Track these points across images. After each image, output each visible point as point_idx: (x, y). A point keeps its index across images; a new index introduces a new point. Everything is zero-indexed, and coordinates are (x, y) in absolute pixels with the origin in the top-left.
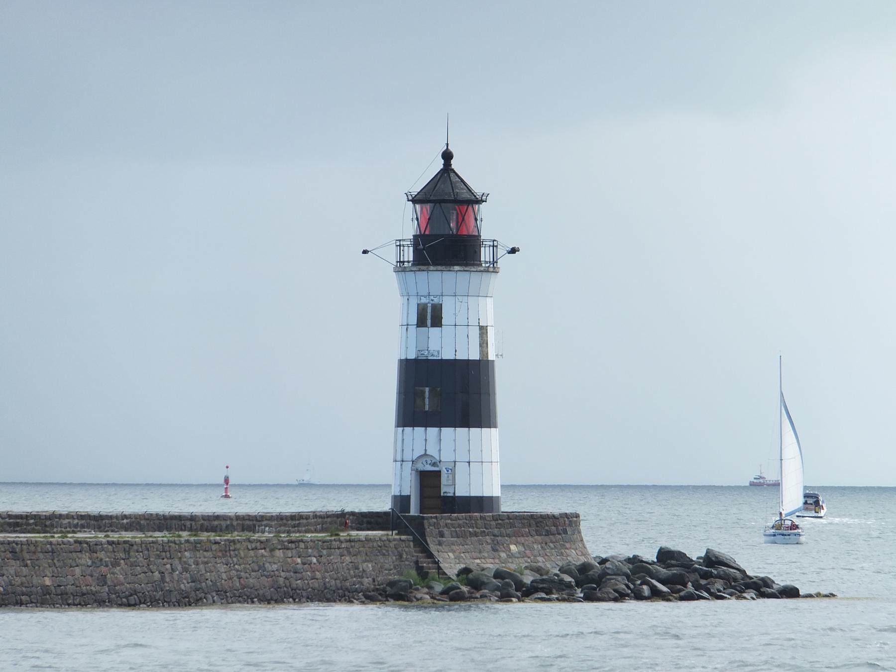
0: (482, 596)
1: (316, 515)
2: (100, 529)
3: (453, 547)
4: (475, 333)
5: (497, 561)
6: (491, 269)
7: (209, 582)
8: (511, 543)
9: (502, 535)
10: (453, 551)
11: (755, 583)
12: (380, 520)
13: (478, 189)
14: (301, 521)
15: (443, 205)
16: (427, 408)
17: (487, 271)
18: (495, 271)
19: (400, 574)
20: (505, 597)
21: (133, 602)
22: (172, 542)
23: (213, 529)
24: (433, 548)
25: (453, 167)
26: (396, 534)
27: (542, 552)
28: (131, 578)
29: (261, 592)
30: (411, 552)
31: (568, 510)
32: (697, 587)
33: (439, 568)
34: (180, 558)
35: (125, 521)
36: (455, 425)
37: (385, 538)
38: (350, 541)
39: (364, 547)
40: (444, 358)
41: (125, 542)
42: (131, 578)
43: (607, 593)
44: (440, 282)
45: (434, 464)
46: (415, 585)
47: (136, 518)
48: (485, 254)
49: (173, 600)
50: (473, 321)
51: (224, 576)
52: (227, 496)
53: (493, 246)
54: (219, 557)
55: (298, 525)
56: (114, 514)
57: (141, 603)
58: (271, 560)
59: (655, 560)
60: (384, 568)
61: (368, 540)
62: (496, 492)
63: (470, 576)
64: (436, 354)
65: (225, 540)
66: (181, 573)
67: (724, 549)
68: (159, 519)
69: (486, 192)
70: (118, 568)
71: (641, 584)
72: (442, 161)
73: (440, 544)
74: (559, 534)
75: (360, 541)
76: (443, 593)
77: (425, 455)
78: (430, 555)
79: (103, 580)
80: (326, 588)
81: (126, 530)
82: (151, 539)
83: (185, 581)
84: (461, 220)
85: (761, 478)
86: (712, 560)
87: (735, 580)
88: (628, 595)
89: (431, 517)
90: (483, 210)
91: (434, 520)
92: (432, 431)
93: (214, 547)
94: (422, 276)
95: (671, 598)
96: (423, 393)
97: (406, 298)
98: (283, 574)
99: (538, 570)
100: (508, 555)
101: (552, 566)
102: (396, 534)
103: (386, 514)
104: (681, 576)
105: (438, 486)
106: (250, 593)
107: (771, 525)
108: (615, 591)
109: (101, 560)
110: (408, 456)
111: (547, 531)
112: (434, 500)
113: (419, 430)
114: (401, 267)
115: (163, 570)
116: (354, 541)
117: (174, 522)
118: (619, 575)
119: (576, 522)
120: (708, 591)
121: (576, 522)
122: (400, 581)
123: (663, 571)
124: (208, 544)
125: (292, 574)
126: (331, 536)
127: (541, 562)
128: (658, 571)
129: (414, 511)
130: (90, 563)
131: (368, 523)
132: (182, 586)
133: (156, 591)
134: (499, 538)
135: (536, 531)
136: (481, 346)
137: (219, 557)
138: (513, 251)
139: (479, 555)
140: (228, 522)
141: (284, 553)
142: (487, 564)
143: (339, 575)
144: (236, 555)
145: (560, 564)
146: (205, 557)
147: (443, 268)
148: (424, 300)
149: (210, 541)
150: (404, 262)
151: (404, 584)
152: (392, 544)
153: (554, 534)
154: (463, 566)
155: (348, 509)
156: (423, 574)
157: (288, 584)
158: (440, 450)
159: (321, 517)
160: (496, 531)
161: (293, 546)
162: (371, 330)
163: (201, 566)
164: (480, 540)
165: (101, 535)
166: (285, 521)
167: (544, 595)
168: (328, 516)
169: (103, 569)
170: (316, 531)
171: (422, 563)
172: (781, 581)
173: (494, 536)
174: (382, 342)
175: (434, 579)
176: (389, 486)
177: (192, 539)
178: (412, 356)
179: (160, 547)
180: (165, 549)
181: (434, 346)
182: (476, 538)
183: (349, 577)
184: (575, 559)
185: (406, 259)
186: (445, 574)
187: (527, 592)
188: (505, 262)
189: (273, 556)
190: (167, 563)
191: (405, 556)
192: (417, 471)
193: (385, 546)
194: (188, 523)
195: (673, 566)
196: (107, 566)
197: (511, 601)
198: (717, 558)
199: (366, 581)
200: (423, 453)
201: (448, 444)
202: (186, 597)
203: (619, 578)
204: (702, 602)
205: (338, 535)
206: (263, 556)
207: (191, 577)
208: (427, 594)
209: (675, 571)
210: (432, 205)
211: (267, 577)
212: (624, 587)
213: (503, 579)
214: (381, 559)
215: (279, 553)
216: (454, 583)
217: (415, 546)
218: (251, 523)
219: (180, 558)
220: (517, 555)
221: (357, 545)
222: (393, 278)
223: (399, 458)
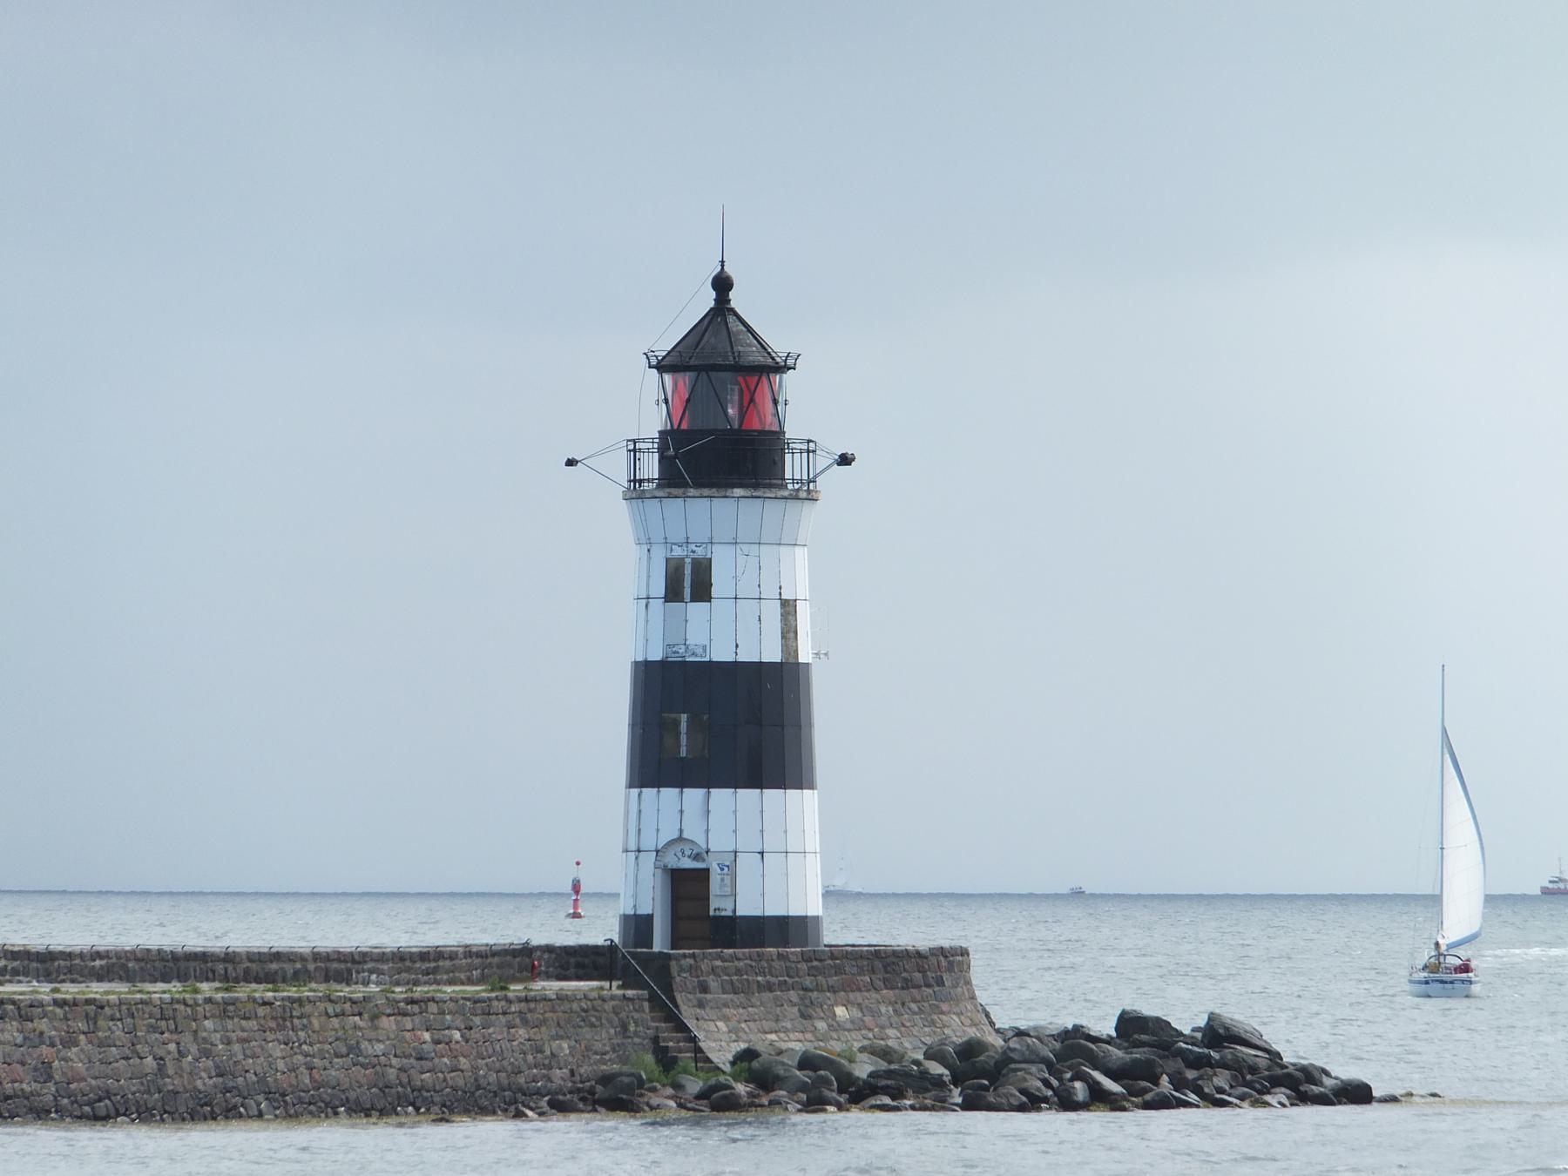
0: (771, 1103)
1: (469, 952)
2: (48, 976)
3: (726, 1011)
4: (773, 612)
5: (809, 1036)
6: (803, 495)
7: (251, 1077)
9: (818, 988)
10: (726, 1019)
11: (1289, 1075)
12: (601, 960)
13: (779, 345)
14: (441, 963)
15: (713, 374)
16: (683, 752)
17: (795, 497)
18: (811, 497)
19: (624, 1060)
20: (814, 1104)
21: (103, 1113)
22: (178, 1002)
23: (269, 979)
24: (688, 1014)
25: (733, 304)
26: (619, 987)
27: (895, 1020)
28: (98, 1068)
29: (352, 1095)
30: (645, 1021)
32: (1179, 1083)
33: (698, 1050)
34: (196, 1032)
35: (98, 963)
36: (735, 784)
37: (594, 994)
38: (526, 1000)
39: (553, 1011)
40: (715, 659)
41: (88, 1002)
42: (98, 1068)
43: (1006, 1096)
44: (706, 518)
46: (650, 1080)
47: (119, 958)
48: (793, 467)
49: (182, 1109)
50: (769, 591)
51: (281, 1065)
52: (576, 915)
53: (808, 451)
54: (271, 1029)
55: (435, 970)
56: (77, 949)
57: (118, 1114)
58: (372, 1035)
59: (1114, 1034)
60: (597, 1050)
61: (562, 998)
62: (812, 905)
63: (755, 1064)
65: (283, 999)
66: (197, 1060)
67: (1239, 1014)
68: (163, 960)
69: (794, 351)
70: (75, 1050)
71: (1072, 1080)
72: (713, 294)
73: (701, 1005)
74: (928, 986)
75: (545, 999)
76: (700, 1096)
77: (681, 839)
78: (682, 1027)
79: (44, 1071)
80: (478, 1087)
81: (100, 979)
82: (138, 996)
83: (204, 1075)
84: (748, 403)
85: (1561, 880)
86: (1218, 1034)
87: (1253, 1069)
88: (1046, 1100)
89: (685, 956)
91: (691, 961)
92: (694, 795)
93: (261, 1011)
94: (674, 507)
96: (677, 723)
97: (645, 548)
98: (394, 1061)
99: (885, 1054)
100: (830, 1026)
101: (911, 1045)
102: (619, 987)
103: (612, 948)
104: (1149, 1064)
106: (331, 1096)
107: (1420, 963)
108: (1023, 1092)
109: (41, 1034)
110: (649, 842)
111: (905, 980)
113: (669, 793)
114: (636, 489)
115: (161, 1053)
116: (534, 1000)
117: (192, 964)
118: (1033, 1062)
119: (960, 963)
120: (1199, 1091)
121: (960, 963)
122: (621, 1074)
123: (1117, 1054)
124: (250, 1006)
125: (412, 1060)
126: (492, 990)
127: (893, 1039)
128: (1107, 1054)
129: (659, 944)
130: (19, 1040)
131: (579, 965)
132: (199, 1083)
133: (148, 1092)
135: (885, 980)
137: (271, 1029)
138: (845, 460)
139: (773, 1025)
140: (298, 965)
141: (398, 1023)
142: (789, 1042)
143: (505, 1063)
144: (304, 1027)
145: (928, 1040)
146: (243, 1030)
147: (713, 491)
148: (678, 552)
149: (254, 1000)
150: (641, 481)
151: (626, 1080)
152: (609, 1006)
153: (919, 987)
154: (743, 1046)
155: (539, 939)
156: (666, 1061)
157: (405, 1080)
159: (479, 955)
160: (808, 981)
161: (416, 1008)
162: (586, 613)
163: (237, 1047)
164: (776, 998)
165: (46, 987)
166: (408, 963)
167: (887, 1100)
168: (494, 954)
169: (45, 1050)
170: (470, 982)
172: (1344, 1070)
173: (805, 989)
174: (610, 631)
175: (685, 1071)
176: (617, 895)
177: (219, 996)
178: (656, 655)
179: (157, 1011)
180: (166, 1013)
181: (696, 637)
182: (770, 995)
183: (524, 1067)
184: (957, 1030)
185: (797, 477)
186: (708, 1060)
187: (858, 1094)
188: (832, 482)
189: (376, 1028)
190: (170, 1041)
191: (632, 1028)
192: (665, 869)
194: (220, 967)
195: (1143, 1044)
196: (53, 1045)
198: (1227, 1029)
199: (557, 1073)
200: (676, 835)
201: (723, 818)
202: (206, 1104)
203: (1033, 1069)
204: (1182, 1112)
205: (504, 988)
206: (356, 1027)
207: (217, 1067)
208: (671, 1097)
209: (1138, 1054)
210: (693, 374)
211: (364, 1066)
212: (1039, 1084)
213: (815, 1069)
214: (586, 1032)
215: (387, 1023)
216: (722, 1078)
218: (343, 966)
219: (196, 1032)
220: (848, 1026)
222: (620, 513)
223: (633, 846)
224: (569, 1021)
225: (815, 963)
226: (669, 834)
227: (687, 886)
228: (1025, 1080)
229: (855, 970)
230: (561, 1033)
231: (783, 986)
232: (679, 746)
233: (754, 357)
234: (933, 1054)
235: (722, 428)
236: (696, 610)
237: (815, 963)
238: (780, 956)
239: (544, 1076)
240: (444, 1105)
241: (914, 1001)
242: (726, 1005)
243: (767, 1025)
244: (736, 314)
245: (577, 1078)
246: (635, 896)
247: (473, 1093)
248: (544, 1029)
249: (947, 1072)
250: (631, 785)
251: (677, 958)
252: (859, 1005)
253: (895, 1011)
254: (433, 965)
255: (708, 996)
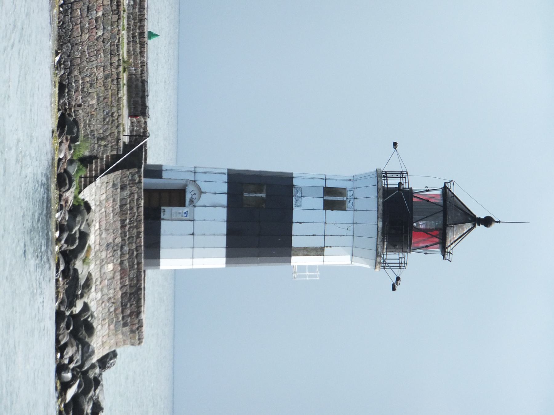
3: (111, 200)
4: (317, 242)
5: (98, 247)
8: (115, 265)
9: (122, 254)
10: (107, 199)
14: (138, 46)
16: (246, 195)
17: (378, 255)
27: (106, 298)
31: (145, 329)
36: (229, 221)
40: (294, 211)
44: (367, 210)
45: (191, 201)
48: (392, 257)
50: (329, 241)
55: (134, 42)
60: (90, 121)
64: (298, 204)
72: (482, 217)
73: (114, 185)
76: (65, 171)
77: (201, 192)
90: (435, 254)
92: (223, 199)
94: (373, 192)
95: (60, 400)
96: (261, 192)
97: (352, 178)
102: (124, 143)
105: (170, 204)
108: (66, 345)
110: (199, 177)
111: (126, 305)
112: (157, 203)
113: (224, 188)
114: (384, 175)
134: (119, 252)
136: (305, 248)
139: (103, 227)
143: (85, 63)
148: (349, 194)
153: (123, 312)
154: (93, 208)
156: (85, 161)
158: (205, 206)
160: (126, 248)
161: (115, 7)
167: (62, 268)
171: (96, 163)
178: (296, 182)
181: (306, 202)
182: (119, 226)
188: (389, 276)
191: (103, 143)
193: (113, 121)
197: (57, 54)
200: (203, 190)
201: (212, 214)
208: (65, 156)
214: (101, 116)
217: (112, 156)
220: (103, 271)
221: (114, 87)
222: (372, 169)
223: (197, 170)
224: (107, 105)
225: (135, 253)
226: (204, 187)
227: (177, 196)
228: (72, 346)
229: (131, 276)
230: (101, 99)
231: (123, 234)
232: (250, 193)
233: (452, 235)
234: (86, 307)
235: (413, 219)
236: (320, 202)
237: (135, 253)
238: (139, 233)
239: (78, 88)
240: (63, 23)
241: (115, 310)
242: (114, 200)
243: (104, 223)
244: (470, 230)
245: (77, 109)
246: (171, 170)
247: (69, 42)
248: (103, 89)
249: (77, 312)
250: (228, 170)
251: (139, 172)
252: (114, 278)
253: (110, 298)
254: (138, 40)
255: (119, 190)
